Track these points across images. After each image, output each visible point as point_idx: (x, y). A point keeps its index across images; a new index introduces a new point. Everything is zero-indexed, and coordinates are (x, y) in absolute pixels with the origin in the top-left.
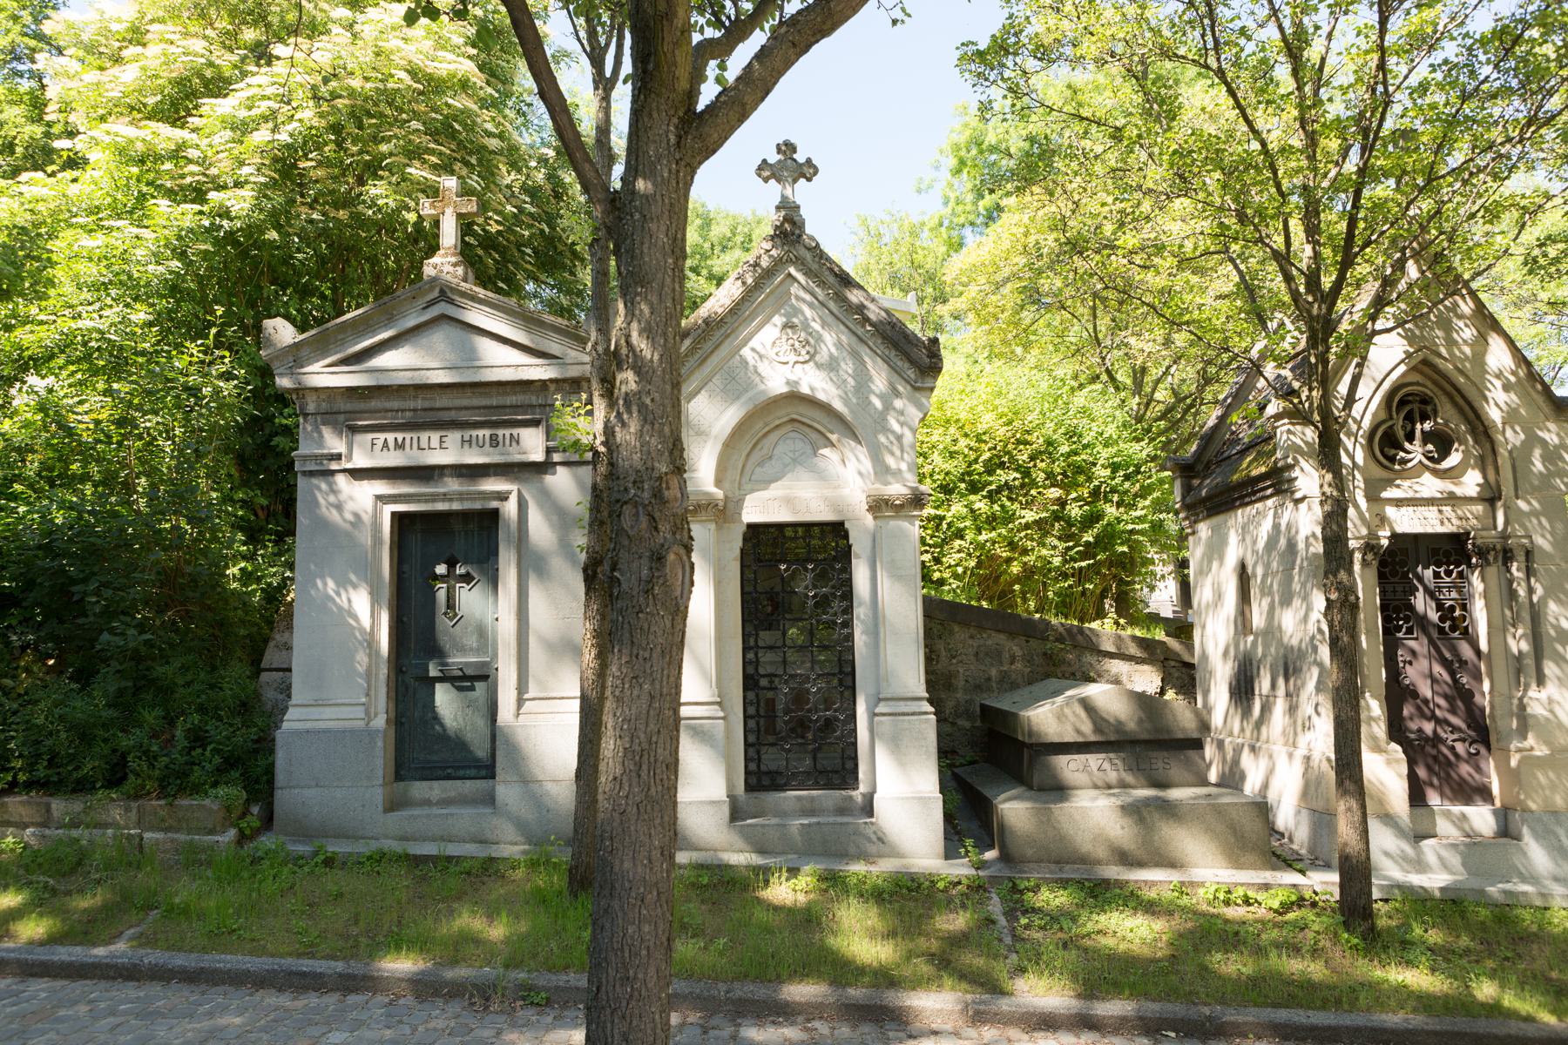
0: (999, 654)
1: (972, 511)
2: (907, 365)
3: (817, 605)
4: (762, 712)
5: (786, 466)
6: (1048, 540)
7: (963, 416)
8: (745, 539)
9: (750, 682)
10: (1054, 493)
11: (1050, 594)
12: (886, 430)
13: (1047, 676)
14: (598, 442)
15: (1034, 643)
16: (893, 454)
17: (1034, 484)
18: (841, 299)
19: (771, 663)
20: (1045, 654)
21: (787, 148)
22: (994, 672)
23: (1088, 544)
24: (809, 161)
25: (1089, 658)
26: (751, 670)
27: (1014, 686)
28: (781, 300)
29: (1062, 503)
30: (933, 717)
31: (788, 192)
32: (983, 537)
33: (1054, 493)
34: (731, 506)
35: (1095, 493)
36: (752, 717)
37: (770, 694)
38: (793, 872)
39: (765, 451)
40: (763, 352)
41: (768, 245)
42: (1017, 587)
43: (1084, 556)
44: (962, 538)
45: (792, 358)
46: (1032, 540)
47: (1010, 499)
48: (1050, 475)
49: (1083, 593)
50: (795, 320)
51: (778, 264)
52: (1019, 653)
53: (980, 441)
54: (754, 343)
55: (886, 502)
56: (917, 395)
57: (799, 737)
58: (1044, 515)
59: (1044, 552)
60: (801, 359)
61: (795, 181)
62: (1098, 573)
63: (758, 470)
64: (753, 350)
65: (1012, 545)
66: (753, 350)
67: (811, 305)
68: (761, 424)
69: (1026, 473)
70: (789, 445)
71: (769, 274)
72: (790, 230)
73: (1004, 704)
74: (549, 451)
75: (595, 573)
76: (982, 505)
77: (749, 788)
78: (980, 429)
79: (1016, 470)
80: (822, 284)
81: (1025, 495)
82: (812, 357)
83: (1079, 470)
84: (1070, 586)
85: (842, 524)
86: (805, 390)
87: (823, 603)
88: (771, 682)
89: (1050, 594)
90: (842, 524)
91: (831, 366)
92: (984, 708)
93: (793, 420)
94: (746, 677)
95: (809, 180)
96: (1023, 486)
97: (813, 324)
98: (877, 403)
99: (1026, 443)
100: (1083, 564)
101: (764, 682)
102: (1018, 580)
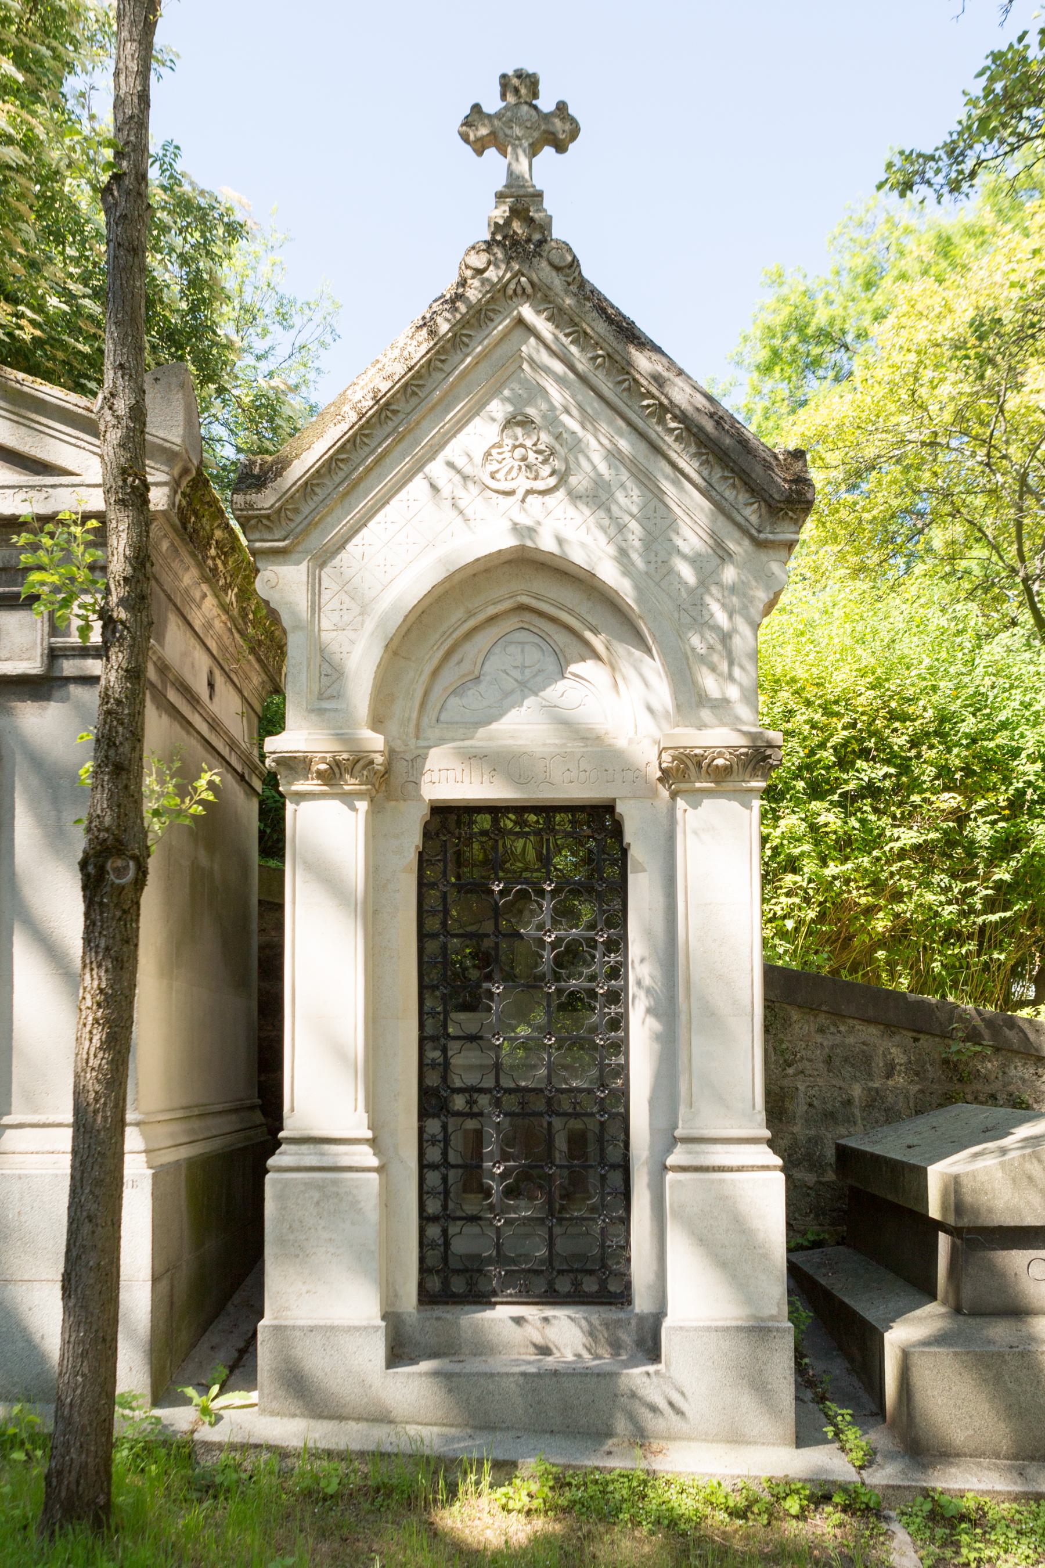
0: (867, 1060)
1: (813, 828)
2: (743, 497)
3: (558, 961)
4: (452, 1158)
5: (507, 694)
6: (936, 879)
7: (801, 673)
8: (427, 834)
9: (432, 1101)
10: (950, 801)
11: (936, 966)
12: (702, 623)
13: (948, 1099)
14: (114, 599)
15: (925, 1042)
16: (713, 669)
17: (915, 785)
18: (621, 368)
19: (470, 1068)
20: (946, 1062)
21: (521, 85)
22: (857, 1091)
23: (999, 885)
24: (562, 107)
25: (1020, 1070)
26: (433, 1080)
27: (891, 1117)
28: (505, 371)
29: (961, 818)
30: (781, 1176)
31: (522, 166)
32: (833, 869)
33: (950, 801)
34: (400, 767)
35: (1016, 804)
36: (434, 1167)
37: (471, 1124)
38: (505, 1470)
39: (466, 666)
40: (468, 470)
41: (479, 261)
42: (881, 954)
43: (991, 904)
44: (795, 870)
45: (522, 483)
46: (910, 877)
47: (876, 810)
48: (944, 771)
49: (986, 967)
50: (531, 411)
51: (500, 296)
52: (901, 1058)
53: (828, 713)
54: (453, 451)
55: (699, 762)
56: (763, 556)
57: (524, 1182)
58: (934, 835)
59: (930, 897)
60: (540, 485)
61: (534, 151)
62: (1011, 935)
63: (454, 701)
64: (450, 465)
65: (876, 885)
66: (450, 465)
67: (560, 380)
68: (460, 613)
69: (904, 768)
70: (508, 655)
71: (479, 317)
72: (523, 235)
73: (888, 1144)
74: (54, 655)
75: (101, 870)
76: (830, 818)
77: (426, 1297)
78: (832, 691)
79: (888, 762)
80: (581, 338)
81: (900, 804)
82: (562, 477)
83: (990, 764)
84: (969, 953)
85: (608, 808)
86: (547, 544)
87: (571, 956)
88: (471, 1102)
89: (936, 966)
90: (608, 808)
91: (597, 497)
92: (844, 1154)
93: (522, 608)
94: (425, 1093)
95: (561, 148)
96: (897, 788)
97: (565, 418)
98: (687, 573)
99: (904, 718)
100: (994, 918)
101: (459, 1102)
102: (882, 943)
